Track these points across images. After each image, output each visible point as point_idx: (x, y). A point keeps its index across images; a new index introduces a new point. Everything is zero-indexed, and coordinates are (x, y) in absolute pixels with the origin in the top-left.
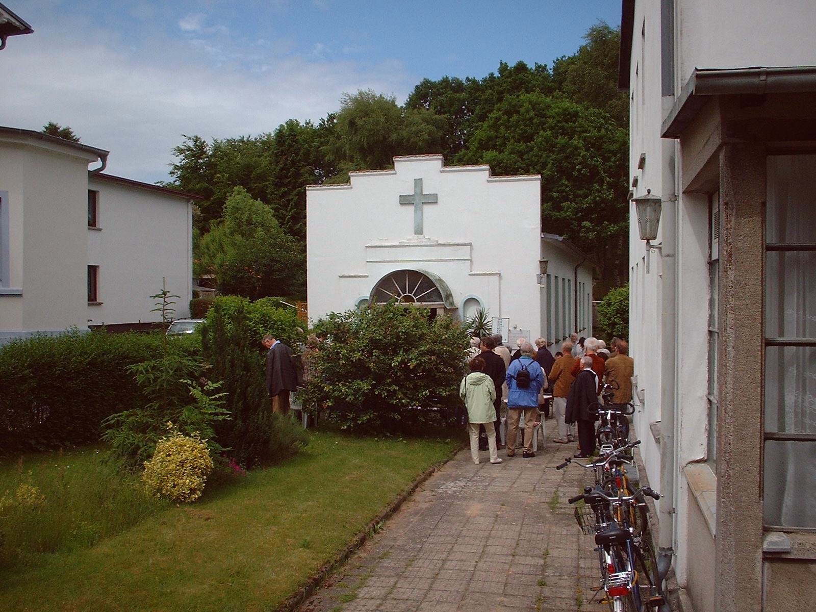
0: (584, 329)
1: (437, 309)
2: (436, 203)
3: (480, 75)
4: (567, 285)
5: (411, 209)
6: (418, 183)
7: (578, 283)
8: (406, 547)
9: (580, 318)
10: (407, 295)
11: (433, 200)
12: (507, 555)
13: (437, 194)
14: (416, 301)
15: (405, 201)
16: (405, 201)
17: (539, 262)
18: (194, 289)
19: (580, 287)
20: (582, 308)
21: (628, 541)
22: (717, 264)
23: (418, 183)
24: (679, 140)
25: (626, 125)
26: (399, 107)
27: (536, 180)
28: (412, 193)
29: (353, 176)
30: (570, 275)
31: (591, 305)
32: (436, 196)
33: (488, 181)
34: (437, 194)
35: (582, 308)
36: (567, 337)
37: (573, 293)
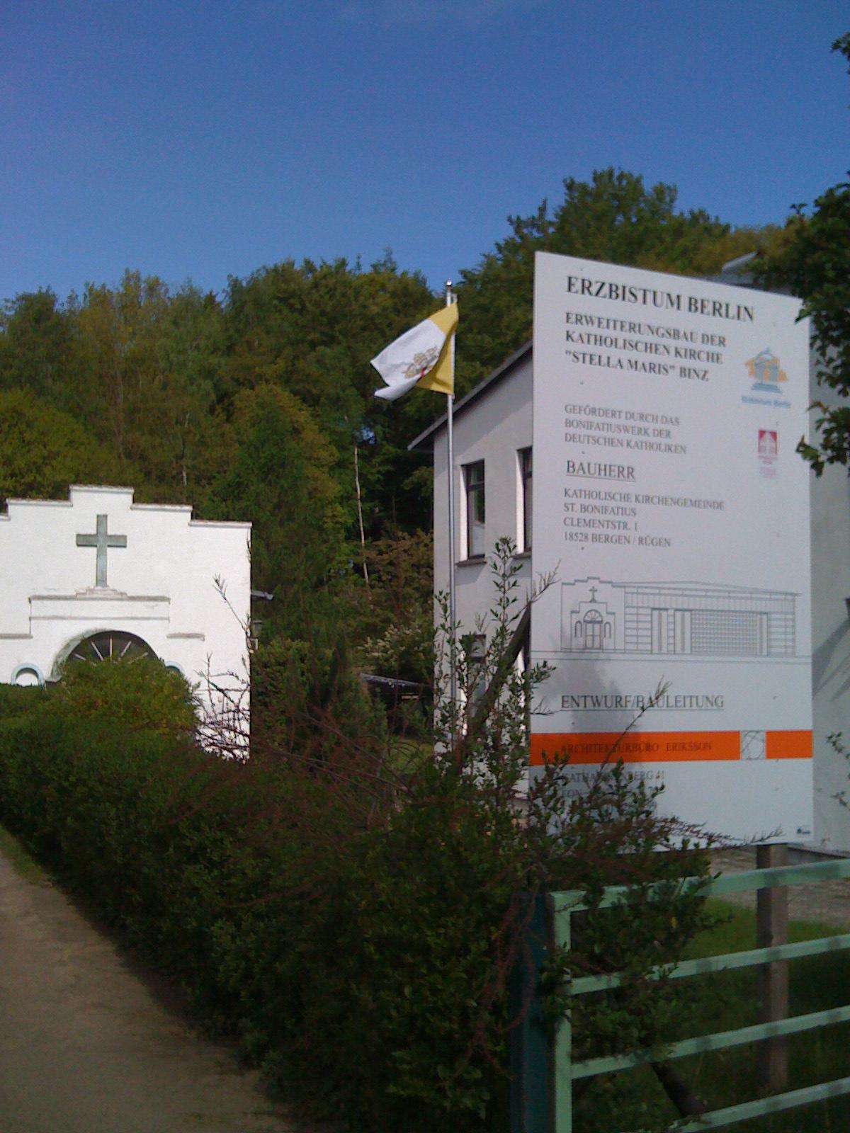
2: (125, 547)
3: (215, 285)
5: (92, 551)
6: (102, 520)
11: (119, 542)
13: (98, 516)
15: (84, 541)
16: (84, 541)
18: (775, 966)
21: (560, 898)
22: (649, 770)
23: (102, 520)
24: (791, 915)
25: (530, 302)
27: (246, 527)
28: (93, 531)
29: (11, 504)
32: (124, 537)
34: (98, 516)
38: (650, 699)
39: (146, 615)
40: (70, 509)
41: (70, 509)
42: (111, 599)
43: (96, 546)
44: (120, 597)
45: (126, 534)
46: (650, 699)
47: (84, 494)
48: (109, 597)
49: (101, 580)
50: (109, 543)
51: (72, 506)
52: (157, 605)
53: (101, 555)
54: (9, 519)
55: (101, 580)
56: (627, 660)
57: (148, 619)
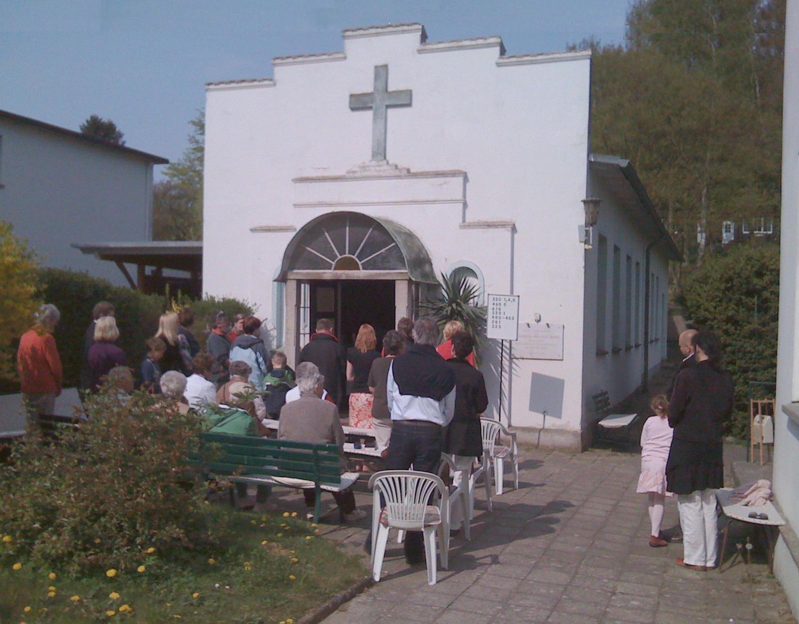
0: (657, 340)
1: (396, 282)
2: (409, 105)
4: (634, 266)
5: (367, 116)
6: (381, 72)
7: (650, 275)
8: (764, 354)
9: (652, 312)
10: (358, 264)
11: (404, 100)
12: (646, 461)
13: (376, 67)
14: (361, 267)
15: (359, 103)
16: (359, 103)
17: (582, 203)
19: (653, 281)
20: (655, 309)
23: (381, 72)
26: (673, 429)
27: (583, 58)
28: (369, 89)
30: (638, 256)
31: (666, 310)
32: (409, 93)
33: (499, 65)
34: (376, 67)
35: (655, 309)
36: (632, 347)
37: (642, 284)
38: (750, 501)
39: (432, 198)
40: (342, 63)
41: (343, 63)
42: (380, 177)
43: (370, 108)
44: (398, 173)
45: (412, 88)
46: (750, 501)
47: (387, 38)
48: (383, 174)
49: (380, 152)
50: (388, 103)
51: (345, 58)
52: (446, 183)
53: (381, 121)
54: (275, 85)
55: (380, 152)
56: (234, 419)
57: (434, 202)
